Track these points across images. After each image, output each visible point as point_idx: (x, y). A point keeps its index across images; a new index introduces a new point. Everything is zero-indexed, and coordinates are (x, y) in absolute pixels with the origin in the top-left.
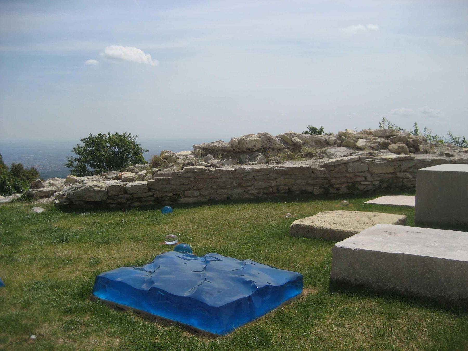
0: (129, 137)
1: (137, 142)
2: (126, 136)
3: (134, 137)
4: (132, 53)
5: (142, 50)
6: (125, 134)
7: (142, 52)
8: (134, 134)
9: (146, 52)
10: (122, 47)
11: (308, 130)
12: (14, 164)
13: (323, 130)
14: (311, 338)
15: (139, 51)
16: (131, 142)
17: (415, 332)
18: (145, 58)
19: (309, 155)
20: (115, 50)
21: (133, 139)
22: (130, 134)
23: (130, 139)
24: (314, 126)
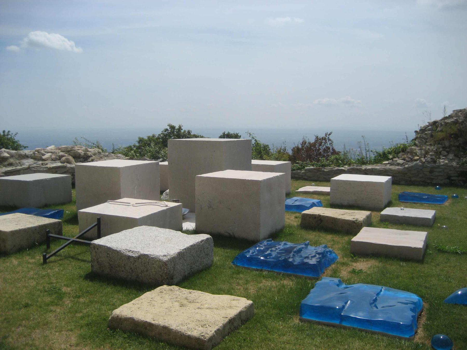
0: (8, 135)
1: (16, 139)
2: (6, 133)
3: (14, 134)
4: (53, 39)
5: (66, 37)
6: (4, 132)
7: (66, 40)
8: (13, 132)
9: (70, 39)
10: (46, 33)
11: (168, 128)
12: (317, 137)
13: (182, 128)
14: (324, 245)
15: (63, 38)
16: (9, 139)
17: (153, 302)
18: (68, 45)
19: (11, 165)
20: (39, 36)
21: (13, 136)
22: (9, 132)
23: (9, 136)
24: (173, 124)
